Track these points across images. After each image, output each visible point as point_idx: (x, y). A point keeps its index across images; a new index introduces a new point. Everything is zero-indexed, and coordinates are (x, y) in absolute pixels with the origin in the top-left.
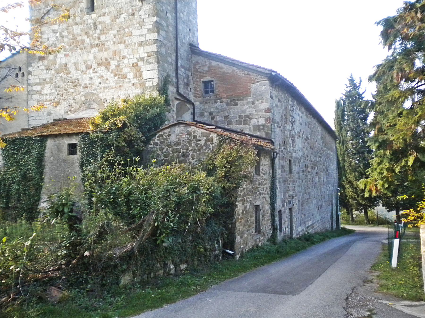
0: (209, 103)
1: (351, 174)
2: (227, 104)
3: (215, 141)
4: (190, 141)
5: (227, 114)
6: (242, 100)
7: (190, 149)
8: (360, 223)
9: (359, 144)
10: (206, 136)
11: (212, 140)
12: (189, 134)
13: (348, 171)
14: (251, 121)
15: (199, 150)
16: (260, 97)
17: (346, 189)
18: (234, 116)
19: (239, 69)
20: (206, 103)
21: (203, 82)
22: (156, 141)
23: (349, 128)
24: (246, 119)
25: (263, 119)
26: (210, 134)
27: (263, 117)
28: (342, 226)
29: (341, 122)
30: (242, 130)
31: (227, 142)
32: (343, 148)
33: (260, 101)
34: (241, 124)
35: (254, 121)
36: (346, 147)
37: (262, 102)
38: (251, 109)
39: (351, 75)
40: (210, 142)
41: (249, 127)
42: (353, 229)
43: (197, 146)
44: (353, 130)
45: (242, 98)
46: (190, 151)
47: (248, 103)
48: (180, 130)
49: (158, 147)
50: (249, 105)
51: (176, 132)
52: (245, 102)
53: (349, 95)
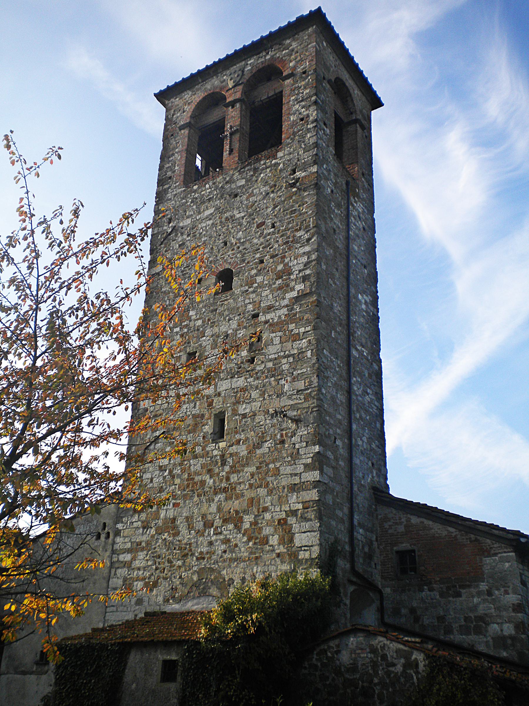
2: (442, 595)
5: (442, 613)
6: (469, 586)
7: (376, 680)
11: (417, 665)
12: (373, 650)
16: (501, 581)
21: (397, 552)
24: (479, 624)
26: (412, 653)
27: (510, 622)
31: (445, 672)
41: (485, 639)
45: (468, 583)
46: (375, 685)
47: (479, 594)
48: (357, 643)
51: (350, 646)
52: (473, 590)
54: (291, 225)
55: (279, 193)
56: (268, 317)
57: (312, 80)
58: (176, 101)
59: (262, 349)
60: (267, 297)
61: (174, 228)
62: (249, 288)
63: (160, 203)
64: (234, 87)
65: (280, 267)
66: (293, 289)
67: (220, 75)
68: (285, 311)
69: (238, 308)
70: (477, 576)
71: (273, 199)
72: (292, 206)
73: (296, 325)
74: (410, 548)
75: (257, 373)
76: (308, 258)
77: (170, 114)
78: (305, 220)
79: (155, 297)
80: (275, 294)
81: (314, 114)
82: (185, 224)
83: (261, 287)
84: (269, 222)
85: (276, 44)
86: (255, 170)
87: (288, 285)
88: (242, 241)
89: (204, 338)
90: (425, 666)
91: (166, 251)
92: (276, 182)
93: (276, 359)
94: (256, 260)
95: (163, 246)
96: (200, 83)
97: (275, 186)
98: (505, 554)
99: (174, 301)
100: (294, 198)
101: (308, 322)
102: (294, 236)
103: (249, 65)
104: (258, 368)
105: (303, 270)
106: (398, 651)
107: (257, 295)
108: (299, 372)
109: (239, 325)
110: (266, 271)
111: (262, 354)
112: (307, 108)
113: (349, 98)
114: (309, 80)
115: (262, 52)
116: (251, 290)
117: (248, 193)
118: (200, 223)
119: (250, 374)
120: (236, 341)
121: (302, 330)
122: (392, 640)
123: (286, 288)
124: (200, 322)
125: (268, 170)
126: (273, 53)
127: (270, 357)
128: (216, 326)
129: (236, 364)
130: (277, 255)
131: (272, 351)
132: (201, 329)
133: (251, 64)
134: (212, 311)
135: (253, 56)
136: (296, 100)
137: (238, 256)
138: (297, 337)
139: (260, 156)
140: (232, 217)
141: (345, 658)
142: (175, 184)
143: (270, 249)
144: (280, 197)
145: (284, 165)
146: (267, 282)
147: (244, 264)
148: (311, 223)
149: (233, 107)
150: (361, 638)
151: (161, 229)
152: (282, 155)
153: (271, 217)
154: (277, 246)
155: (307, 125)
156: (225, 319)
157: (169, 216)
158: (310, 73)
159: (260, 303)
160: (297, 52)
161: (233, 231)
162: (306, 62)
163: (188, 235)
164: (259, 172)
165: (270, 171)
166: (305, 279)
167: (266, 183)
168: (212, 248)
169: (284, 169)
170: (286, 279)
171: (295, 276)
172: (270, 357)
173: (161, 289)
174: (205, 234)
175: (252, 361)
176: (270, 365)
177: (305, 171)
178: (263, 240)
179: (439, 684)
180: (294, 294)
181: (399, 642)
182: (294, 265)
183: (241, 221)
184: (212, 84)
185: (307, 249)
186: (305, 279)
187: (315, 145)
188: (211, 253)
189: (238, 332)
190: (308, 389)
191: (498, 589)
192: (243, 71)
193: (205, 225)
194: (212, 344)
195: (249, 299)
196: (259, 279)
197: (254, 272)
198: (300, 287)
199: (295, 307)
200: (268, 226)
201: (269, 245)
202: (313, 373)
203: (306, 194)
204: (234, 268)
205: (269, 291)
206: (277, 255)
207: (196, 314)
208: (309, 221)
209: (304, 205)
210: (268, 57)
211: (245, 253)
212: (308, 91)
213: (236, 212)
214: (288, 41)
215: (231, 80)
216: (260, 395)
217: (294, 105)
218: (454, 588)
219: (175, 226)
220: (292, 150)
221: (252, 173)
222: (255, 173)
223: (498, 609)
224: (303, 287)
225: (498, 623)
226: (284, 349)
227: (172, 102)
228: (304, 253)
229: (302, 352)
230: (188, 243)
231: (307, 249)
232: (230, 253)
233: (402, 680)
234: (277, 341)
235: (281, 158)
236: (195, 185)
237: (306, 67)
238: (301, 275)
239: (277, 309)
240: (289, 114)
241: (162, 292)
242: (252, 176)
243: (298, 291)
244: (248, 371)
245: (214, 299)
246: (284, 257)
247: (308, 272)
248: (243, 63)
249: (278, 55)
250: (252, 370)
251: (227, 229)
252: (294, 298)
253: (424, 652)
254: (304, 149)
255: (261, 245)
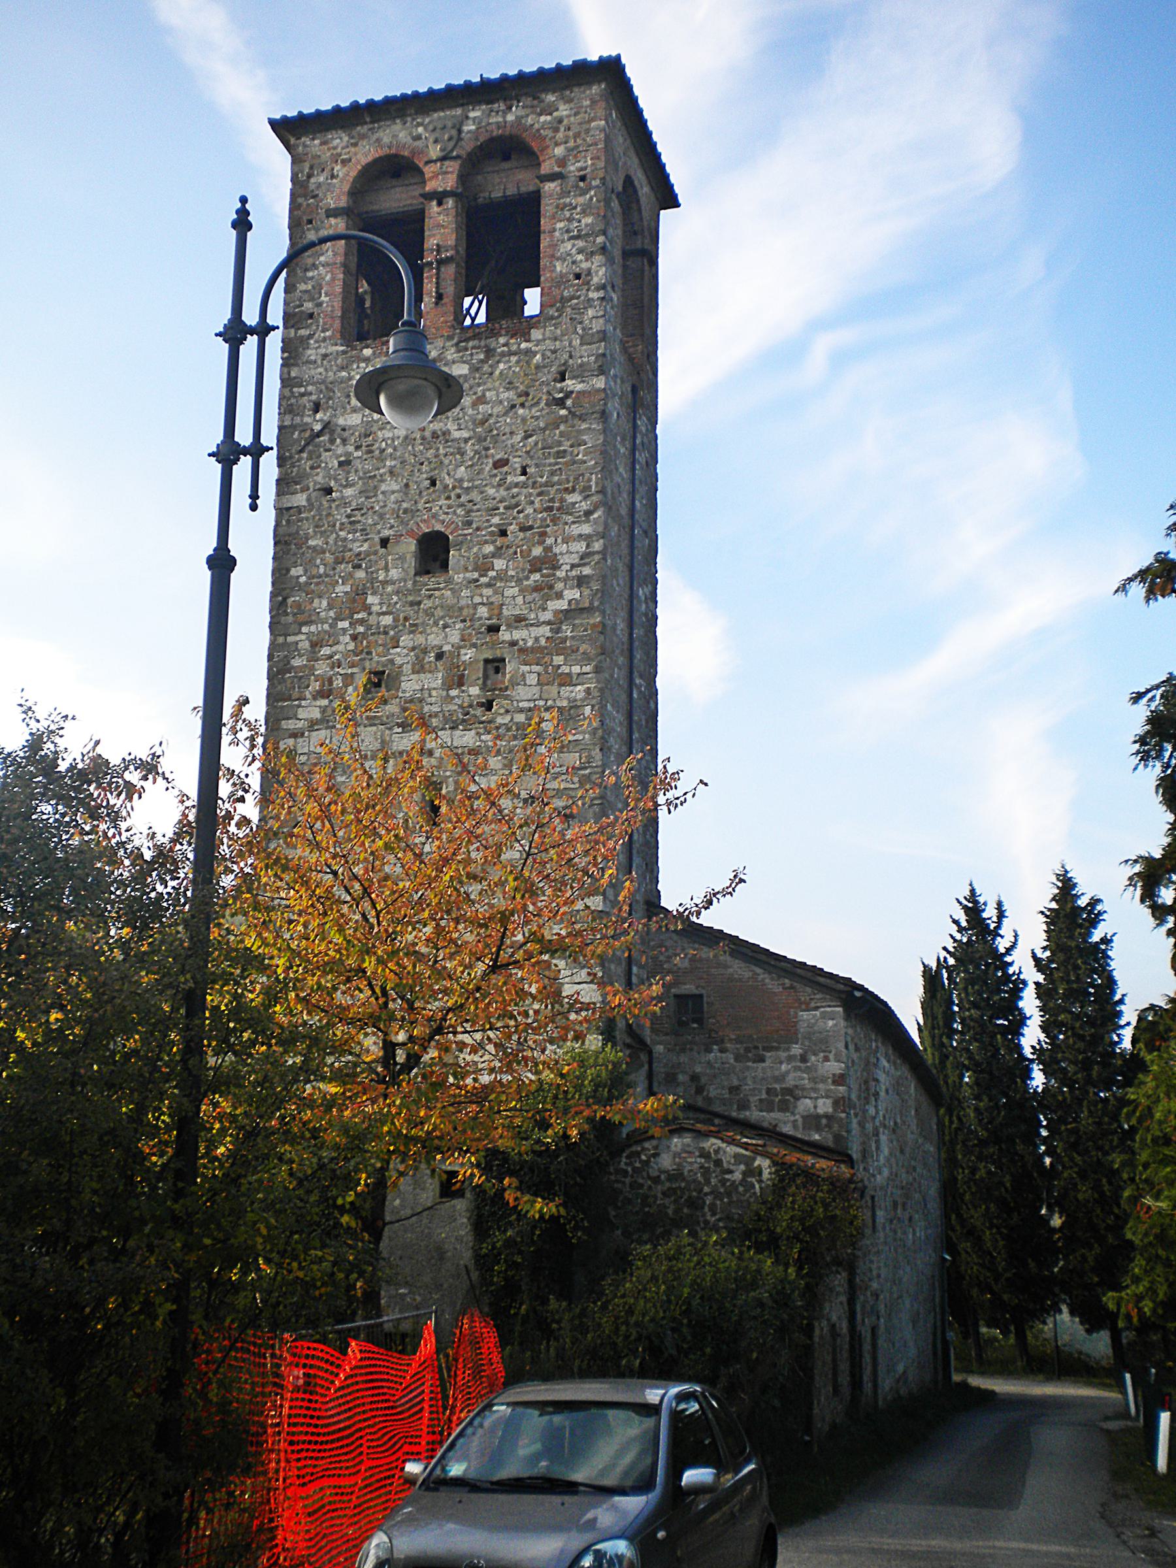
0: (691, 1050)
1: (975, 1207)
2: (737, 1058)
3: (766, 1175)
4: (706, 1172)
5: (736, 1083)
6: (777, 1049)
7: (706, 1189)
8: (1004, 1369)
9: (999, 1113)
10: (747, 1164)
11: (760, 1174)
12: (705, 1154)
13: (967, 1197)
14: (799, 1103)
15: (729, 1194)
16: (819, 1044)
17: (959, 1254)
18: (754, 1089)
19: (770, 973)
20: (683, 1050)
21: (676, 996)
22: (622, 1165)
23: (970, 1058)
24: (787, 1098)
25: (829, 1102)
26: (754, 1159)
27: (827, 1097)
28: (956, 1378)
29: (945, 1040)
30: (776, 1126)
31: (799, 1182)
32: (951, 1122)
33: (822, 1055)
34: (772, 1111)
35: (805, 1105)
36: (959, 1119)
37: (826, 1059)
38: (799, 1074)
39: (973, 891)
40: (754, 1176)
41: (792, 1118)
42: (990, 1387)
43: (723, 1185)
44: (977, 1064)
45: (775, 1044)
46: (706, 1194)
47: (790, 1059)
48: (683, 1144)
49: (628, 1180)
50: (794, 1064)
51: (673, 1148)
52: (783, 1055)
53: (963, 953)
54: (556, 478)
55: (533, 410)
56: (517, 635)
57: (598, 201)
58: (312, 145)
59: (507, 689)
60: (514, 600)
61: (327, 425)
62: (481, 576)
63: (293, 365)
64: (443, 159)
65: (537, 551)
66: (559, 596)
67: (409, 119)
68: (546, 631)
69: (461, 609)
70: (789, 1035)
71: (524, 420)
72: (560, 444)
73: (565, 659)
74: (696, 992)
75: (498, 728)
76: (588, 546)
77: (302, 172)
78: (583, 475)
79: (295, 554)
80: (529, 598)
81: (600, 273)
82: (349, 423)
83: (501, 580)
84: (516, 463)
85: (526, 94)
86: (489, 352)
87: (551, 587)
88: (466, 485)
89: (398, 650)
90: (770, 1173)
91: (312, 468)
92: (528, 387)
93: (530, 710)
94: (493, 528)
95: (305, 455)
96: (366, 123)
97: (527, 394)
98: (828, 1009)
99: (334, 569)
100: (562, 427)
101: (587, 658)
102: (562, 500)
103: (471, 122)
104: (499, 720)
105: (579, 565)
106: (736, 1156)
107: (496, 593)
108: (571, 738)
109: (463, 640)
110: (511, 551)
111: (507, 697)
112: (590, 255)
113: (634, 206)
114: (591, 198)
115: (497, 100)
116: (484, 580)
117: (475, 393)
118: (381, 429)
119: (485, 728)
120: (458, 666)
121: (576, 669)
122: (729, 1143)
123: (546, 590)
124: (387, 620)
125: (514, 359)
126: (521, 112)
127: (521, 705)
128: (421, 633)
129: (461, 707)
130: (531, 528)
131: (524, 694)
132: (392, 633)
133: (477, 120)
134: (412, 604)
135: (480, 103)
136: (568, 231)
137: (458, 511)
138: (567, 680)
139: (497, 325)
140: (444, 434)
141: (666, 1162)
142: (323, 331)
143: (519, 512)
144: (537, 418)
145: (544, 359)
146: (513, 573)
147: (470, 531)
148: (593, 483)
149: (440, 204)
150: (687, 1139)
151: (298, 420)
152: (540, 337)
153: (519, 453)
154: (532, 511)
155: (588, 290)
156: (436, 624)
157: (314, 397)
158: (594, 183)
159: (501, 609)
160: (569, 129)
161: (446, 462)
162: (585, 157)
163: (358, 448)
164: (497, 358)
165: (518, 362)
166: (581, 581)
167: (510, 383)
168: (407, 485)
169: (544, 367)
170: (548, 576)
171: (564, 574)
172: (521, 705)
173: (307, 539)
174: (391, 454)
175: (489, 706)
176: (521, 718)
177: (583, 382)
178: (505, 493)
179: (793, 1195)
180: (562, 605)
181: (737, 1145)
182: (561, 554)
183: (463, 445)
184: (396, 135)
185: (586, 529)
186: (581, 581)
187: (601, 335)
188: (406, 494)
189: (463, 651)
190: (586, 768)
191: (815, 1054)
192: (460, 131)
193: (390, 435)
194: (414, 665)
195: (481, 595)
196: (499, 564)
197: (489, 549)
198: (572, 594)
199: (564, 628)
200: (515, 469)
201: (517, 505)
202: (595, 744)
203: (584, 426)
204: (451, 533)
205: (517, 589)
206: (531, 528)
207: (380, 604)
208: (590, 480)
209: (580, 445)
210: (510, 118)
211: (471, 511)
212: (589, 220)
213: (451, 426)
214: (551, 98)
215: (436, 141)
216: (505, 765)
217: (563, 242)
218: (754, 1052)
219: (329, 422)
220: (559, 332)
221: (482, 356)
222: (488, 358)
223: (813, 1080)
224: (577, 596)
225: (811, 1098)
226: (545, 696)
227: (305, 146)
228: (580, 535)
229: (575, 706)
230: (357, 464)
231: (586, 529)
232: (443, 502)
233: (741, 1189)
234: (532, 679)
235: (538, 342)
236: (367, 347)
237: (586, 168)
238: (574, 573)
239: (532, 625)
240: (553, 256)
241: (309, 547)
242: (482, 361)
243: (570, 602)
244: (482, 722)
245: (415, 582)
246: (543, 534)
247: (587, 571)
248: (459, 111)
249: (530, 121)
250: (490, 722)
251: (436, 456)
252: (562, 611)
253: (770, 1158)
254: (582, 337)
255: (501, 502)
